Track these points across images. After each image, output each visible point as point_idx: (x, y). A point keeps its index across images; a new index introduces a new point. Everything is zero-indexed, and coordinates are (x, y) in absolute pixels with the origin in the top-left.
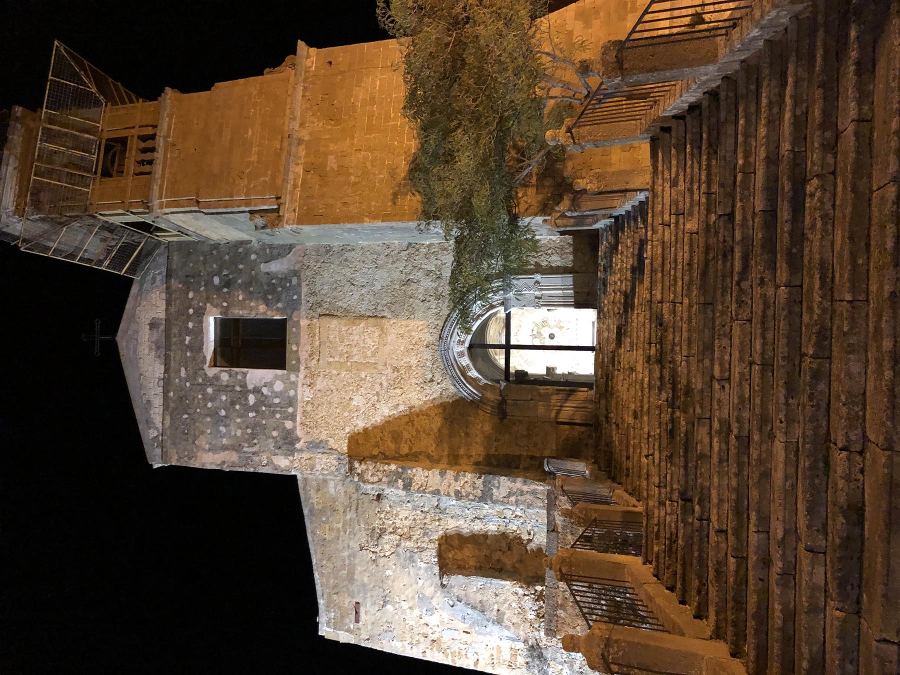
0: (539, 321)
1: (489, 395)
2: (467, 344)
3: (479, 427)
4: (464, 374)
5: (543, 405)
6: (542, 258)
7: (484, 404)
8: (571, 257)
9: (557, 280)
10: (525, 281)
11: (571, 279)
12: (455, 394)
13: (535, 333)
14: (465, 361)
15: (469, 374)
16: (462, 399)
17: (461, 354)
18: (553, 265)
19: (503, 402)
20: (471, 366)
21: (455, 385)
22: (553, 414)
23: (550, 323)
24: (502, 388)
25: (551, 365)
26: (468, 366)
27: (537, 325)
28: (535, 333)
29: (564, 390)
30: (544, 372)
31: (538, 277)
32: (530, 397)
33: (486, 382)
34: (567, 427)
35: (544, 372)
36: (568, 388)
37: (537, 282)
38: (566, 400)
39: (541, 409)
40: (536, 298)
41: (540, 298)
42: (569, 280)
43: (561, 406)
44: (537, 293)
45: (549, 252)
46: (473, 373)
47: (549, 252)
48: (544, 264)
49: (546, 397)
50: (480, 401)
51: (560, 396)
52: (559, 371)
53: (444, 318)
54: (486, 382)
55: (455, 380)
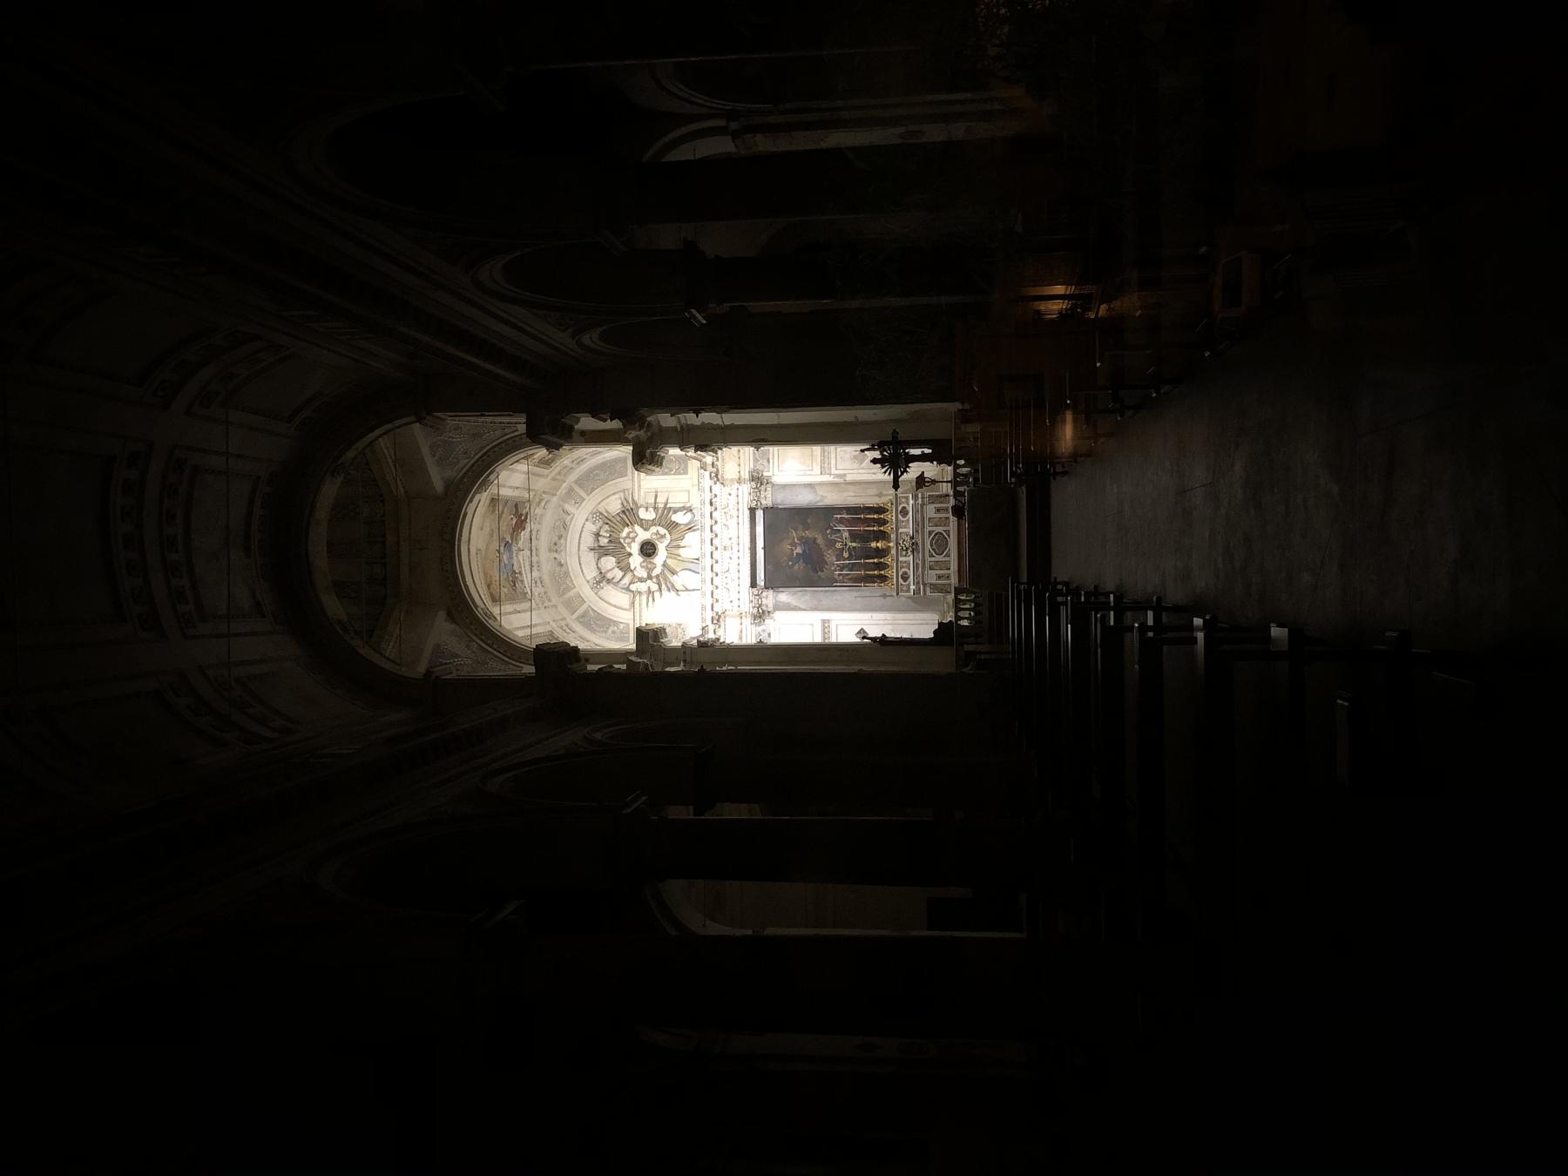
0: (614, 506)
13: (604, 541)
27: (607, 520)
28: (604, 541)
30: (631, 645)
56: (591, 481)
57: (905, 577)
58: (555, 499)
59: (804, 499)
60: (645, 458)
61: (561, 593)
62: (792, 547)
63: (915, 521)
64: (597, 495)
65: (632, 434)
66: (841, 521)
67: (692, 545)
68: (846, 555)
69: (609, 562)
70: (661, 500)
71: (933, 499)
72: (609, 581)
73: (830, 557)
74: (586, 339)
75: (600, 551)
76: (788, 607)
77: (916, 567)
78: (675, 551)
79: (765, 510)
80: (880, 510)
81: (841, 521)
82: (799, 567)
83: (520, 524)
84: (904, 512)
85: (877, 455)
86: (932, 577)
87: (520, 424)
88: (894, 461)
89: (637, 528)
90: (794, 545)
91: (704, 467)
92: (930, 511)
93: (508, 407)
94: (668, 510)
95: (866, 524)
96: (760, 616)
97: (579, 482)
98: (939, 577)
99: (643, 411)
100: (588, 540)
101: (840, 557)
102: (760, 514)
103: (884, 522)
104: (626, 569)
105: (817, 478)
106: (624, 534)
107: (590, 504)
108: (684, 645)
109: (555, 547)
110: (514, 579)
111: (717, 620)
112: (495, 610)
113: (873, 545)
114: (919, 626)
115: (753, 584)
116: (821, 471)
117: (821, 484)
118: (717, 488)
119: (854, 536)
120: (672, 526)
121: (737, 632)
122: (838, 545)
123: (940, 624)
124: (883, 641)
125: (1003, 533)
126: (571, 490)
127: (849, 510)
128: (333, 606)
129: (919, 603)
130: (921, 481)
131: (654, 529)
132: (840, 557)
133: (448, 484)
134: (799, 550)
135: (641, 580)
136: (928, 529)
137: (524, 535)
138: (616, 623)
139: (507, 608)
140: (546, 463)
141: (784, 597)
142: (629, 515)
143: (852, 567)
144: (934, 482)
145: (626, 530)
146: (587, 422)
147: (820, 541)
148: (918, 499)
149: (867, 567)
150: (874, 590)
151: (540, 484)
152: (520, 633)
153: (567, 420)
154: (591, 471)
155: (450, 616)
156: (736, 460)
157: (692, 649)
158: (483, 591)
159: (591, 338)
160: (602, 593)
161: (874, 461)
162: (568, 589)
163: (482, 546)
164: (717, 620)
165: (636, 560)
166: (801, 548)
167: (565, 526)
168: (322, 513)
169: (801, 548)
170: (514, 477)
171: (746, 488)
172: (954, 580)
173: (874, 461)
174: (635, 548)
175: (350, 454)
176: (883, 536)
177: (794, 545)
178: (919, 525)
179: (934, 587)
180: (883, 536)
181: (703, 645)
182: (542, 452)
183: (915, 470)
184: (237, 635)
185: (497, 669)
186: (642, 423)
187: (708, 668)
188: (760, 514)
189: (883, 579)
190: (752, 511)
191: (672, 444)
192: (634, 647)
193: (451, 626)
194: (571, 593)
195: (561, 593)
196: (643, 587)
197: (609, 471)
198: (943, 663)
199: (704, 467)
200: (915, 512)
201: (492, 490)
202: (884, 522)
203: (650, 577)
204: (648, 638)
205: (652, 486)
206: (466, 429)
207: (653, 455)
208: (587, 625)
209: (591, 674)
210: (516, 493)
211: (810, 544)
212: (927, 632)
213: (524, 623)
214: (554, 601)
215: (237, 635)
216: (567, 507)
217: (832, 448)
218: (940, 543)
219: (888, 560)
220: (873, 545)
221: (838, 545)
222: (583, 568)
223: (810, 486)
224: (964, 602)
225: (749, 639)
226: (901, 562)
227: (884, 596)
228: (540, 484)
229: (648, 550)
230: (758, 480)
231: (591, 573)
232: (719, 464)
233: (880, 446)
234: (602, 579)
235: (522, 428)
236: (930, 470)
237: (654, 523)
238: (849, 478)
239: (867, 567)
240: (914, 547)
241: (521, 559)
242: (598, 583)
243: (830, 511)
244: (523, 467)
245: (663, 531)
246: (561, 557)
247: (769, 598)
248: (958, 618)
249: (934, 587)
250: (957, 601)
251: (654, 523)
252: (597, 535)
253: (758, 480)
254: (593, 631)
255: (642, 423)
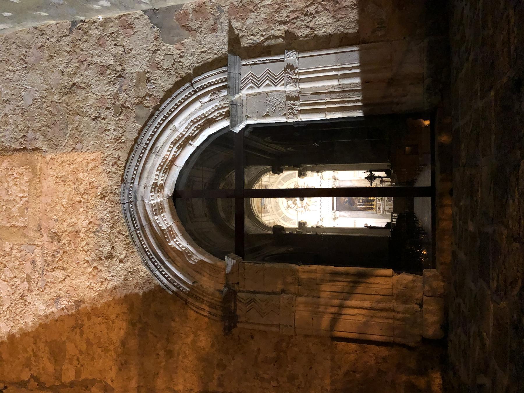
30: (297, 226)
76: (343, 216)
82: (347, 204)
96: (335, 219)
112: (260, 215)
114: (381, 222)
115: (333, 209)
118: (322, 181)
124: (371, 227)
126: (280, 181)
128: (223, 215)
129: (384, 216)
133: (249, 182)
139: (263, 215)
141: (343, 213)
143: (363, 205)
149: (367, 205)
150: (370, 211)
151: (272, 180)
154: (286, 176)
157: (314, 228)
158: (257, 210)
159: (290, 149)
175: (227, 176)
181: (317, 227)
184: (204, 221)
185: (261, 232)
187: (318, 233)
189: (373, 209)
192: (430, 198)
193: (248, 220)
194: (280, 211)
197: (291, 176)
201: (260, 182)
204: (302, 225)
208: (284, 220)
209: (287, 234)
210: (265, 183)
212: (384, 225)
215: (204, 221)
224: (395, 216)
225: (331, 226)
227: (373, 214)
239: (367, 205)
247: (338, 213)
248: (392, 221)
253: (221, 360)
254: (286, 222)
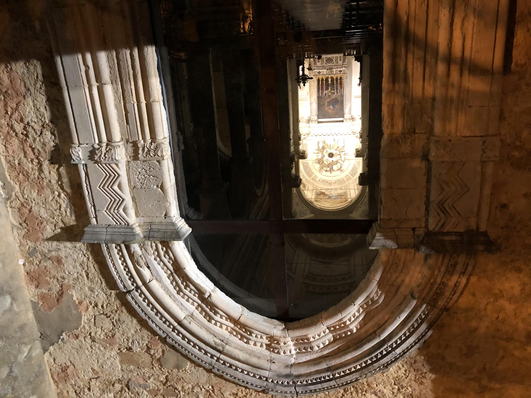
0: (318, 166)
1: (416, 274)
2: (276, 328)
3: (510, 307)
4: (353, 342)
5: (445, 119)
6: (38, 146)
7: (439, 294)
8: (19, 67)
9: (79, 100)
10: (97, 188)
11: (67, 59)
12: (412, 364)
13: (328, 169)
14: (320, 335)
15: (353, 327)
16: (425, 347)
17: (304, 345)
18: (47, 115)
19: (433, 242)
20: (331, 322)
21: (387, 366)
22: (476, 85)
23: (320, 157)
24: (390, 244)
25: (354, 152)
26: (332, 329)
27: (322, 168)
28: (328, 169)
29: (394, 55)
30: (360, 159)
31: (79, 154)
32: (417, 163)
33: (373, 286)
34: (520, 36)
35: (360, 159)
36: (387, 46)
37: (92, 154)
38: (427, 48)
39: (459, 125)
40: (135, 157)
41: (135, 144)
42: (73, 66)
43: (449, 60)
44: (121, 154)
45: (19, 128)
46: (352, 315)
47: (19, 128)
48: (48, 137)
49: (417, 111)
50: (432, 304)
51: (414, 68)
52: (359, 146)
53: (215, 380)
54: (373, 286)
55: (375, 361)
56: (309, 173)
57: (341, 71)
58: (316, 184)
59: (315, 106)
60: (303, 156)
61: (344, 182)
62: (330, 109)
63: (323, 69)
64: (314, 171)
65: (296, 160)
66: (322, 93)
67: (329, 141)
68: (333, 91)
69: (335, 167)
70: (317, 152)
71: (315, 63)
72: (341, 167)
73: (334, 96)
74: (259, 194)
75: (331, 170)
76: (350, 110)
77: (337, 68)
78: (331, 147)
79: (318, 118)
80: (318, 80)
81: (322, 93)
82: (337, 107)
83: (323, 194)
84: (319, 73)
85: (302, 84)
86: (340, 63)
87: (294, 190)
88: (305, 79)
89: (324, 159)
90: (330, 109)
91: (305, 138)
92: (319, 64)
93: (290, 193)
94: (318, 149)
95: (324, 85)
96: (353, 119)
97: (310, 176)
98: (340, 60)
99: (290, 155)
100: (328, 174)
101: (334, 93)
102: (320, 120)
103: (322, 79)
104: (337, 162)
105: (309, 102)
106: (326, 163)
107: (316, 173)
108: (361, 143)
109: (330, 184)
110: (340, 196)
111: (354, 133)
112: (349, 200)
113: (330, 82)
114: (356, 66)
115: (343, 121)
116: (307, 98)
117: (310, 100)
118: (312, 134)
119: (327, 89)
120: (324, 148)
121: (357, 126)
122: (330, 94)
123: (355, 60)
124: (361, 79)
125: (328, 43)
126: (312, 179)
127: (318, 91)
130: (310, 69)
131: (324, 153)
132: (334, 93)
133: (312, 213)
134: (331, 107)
135: (341, 157)
136: (325, 65)
137: (326, 193)
138: (354, 165)
139: (349, 197)
140: (304, 186)
141: (346, 111)
142: (320, 161)
144: (310, 65)
145: (325, 162)
146: (293, 171)
147: (328, 100)
148: (314, 68)
150: (345, 81)
151: (311, 188)
152: (357, 193)
153: (294, 177)
155: (351, 212)
156: (303, 128)
157: (362, 140)
160: (345, 169)
161: (304, 85)
162: (343, 179)
163: (330, 204)
164: (354, 133)
165: (334, 159)
166: (331, 106)
167: (324, 181)
168: (321, 244)
169: (331, 106)
170: (309, 195)
171: (311, 124)
172: (342, 55)
173: (304, 85)
174: (331, 159)
176: (327, 79)
177: (330, 109)
178: (324, 68)
179: (344, 61)
180: (327, 79)
182: (301, 187)
183: (307, 72)
186: (293, 155)
188: (320, 120)
189: (341, 78)
190: (319, 122)
191: (298, 148)
192: (361, 158)
193: (354, 212)
195: (344, 182)
196: (343, 157)
197: (306, 167)
198: (367, 59)
199: (305, 138)
200: (319, 69)
201: (313, 200)
202: (322, 79)
203: (340, 155)
204: (358, 154)
205: (312, 156)
206: (295, 200)
207: (302, 153)
211: (329, 103)
212: (359, 64)
213: (354, 191)
214: (347, 184)
216: (318, 180)
217: (300, 97)
218: (329, 60)
219: (335, 77)
220: (330, 82)
221: (330, 94)
222: (336, 176)
223: (311, 104)
226: (336, 73)
227: (347, 78)
228: (311, 188)
229: (331, 155)
230: (309, 121)
231: (338, 172)
232: (304, 134)
233: (299, 83)
234: (340, 169)
235: (295, 189)
236: (306, 65)
237: (323, 154)
238: (308, 91)
240: (331, 69)
241: (334, 193)
242: (341, 170)
243: (319, 98)
244: (306, 192)
245: (325, 151)
246: (334, 182)
247: (347, 116)
248: (353, 55)
249: (344, 61)
250: (348, 55)
251: (323, 154)
252: (326, 171)
254: (357, 172)
255: (293, 155)
